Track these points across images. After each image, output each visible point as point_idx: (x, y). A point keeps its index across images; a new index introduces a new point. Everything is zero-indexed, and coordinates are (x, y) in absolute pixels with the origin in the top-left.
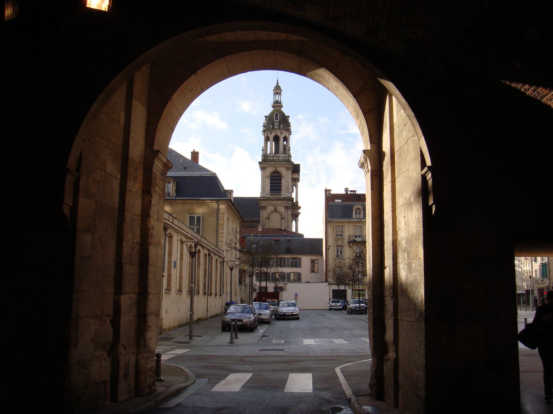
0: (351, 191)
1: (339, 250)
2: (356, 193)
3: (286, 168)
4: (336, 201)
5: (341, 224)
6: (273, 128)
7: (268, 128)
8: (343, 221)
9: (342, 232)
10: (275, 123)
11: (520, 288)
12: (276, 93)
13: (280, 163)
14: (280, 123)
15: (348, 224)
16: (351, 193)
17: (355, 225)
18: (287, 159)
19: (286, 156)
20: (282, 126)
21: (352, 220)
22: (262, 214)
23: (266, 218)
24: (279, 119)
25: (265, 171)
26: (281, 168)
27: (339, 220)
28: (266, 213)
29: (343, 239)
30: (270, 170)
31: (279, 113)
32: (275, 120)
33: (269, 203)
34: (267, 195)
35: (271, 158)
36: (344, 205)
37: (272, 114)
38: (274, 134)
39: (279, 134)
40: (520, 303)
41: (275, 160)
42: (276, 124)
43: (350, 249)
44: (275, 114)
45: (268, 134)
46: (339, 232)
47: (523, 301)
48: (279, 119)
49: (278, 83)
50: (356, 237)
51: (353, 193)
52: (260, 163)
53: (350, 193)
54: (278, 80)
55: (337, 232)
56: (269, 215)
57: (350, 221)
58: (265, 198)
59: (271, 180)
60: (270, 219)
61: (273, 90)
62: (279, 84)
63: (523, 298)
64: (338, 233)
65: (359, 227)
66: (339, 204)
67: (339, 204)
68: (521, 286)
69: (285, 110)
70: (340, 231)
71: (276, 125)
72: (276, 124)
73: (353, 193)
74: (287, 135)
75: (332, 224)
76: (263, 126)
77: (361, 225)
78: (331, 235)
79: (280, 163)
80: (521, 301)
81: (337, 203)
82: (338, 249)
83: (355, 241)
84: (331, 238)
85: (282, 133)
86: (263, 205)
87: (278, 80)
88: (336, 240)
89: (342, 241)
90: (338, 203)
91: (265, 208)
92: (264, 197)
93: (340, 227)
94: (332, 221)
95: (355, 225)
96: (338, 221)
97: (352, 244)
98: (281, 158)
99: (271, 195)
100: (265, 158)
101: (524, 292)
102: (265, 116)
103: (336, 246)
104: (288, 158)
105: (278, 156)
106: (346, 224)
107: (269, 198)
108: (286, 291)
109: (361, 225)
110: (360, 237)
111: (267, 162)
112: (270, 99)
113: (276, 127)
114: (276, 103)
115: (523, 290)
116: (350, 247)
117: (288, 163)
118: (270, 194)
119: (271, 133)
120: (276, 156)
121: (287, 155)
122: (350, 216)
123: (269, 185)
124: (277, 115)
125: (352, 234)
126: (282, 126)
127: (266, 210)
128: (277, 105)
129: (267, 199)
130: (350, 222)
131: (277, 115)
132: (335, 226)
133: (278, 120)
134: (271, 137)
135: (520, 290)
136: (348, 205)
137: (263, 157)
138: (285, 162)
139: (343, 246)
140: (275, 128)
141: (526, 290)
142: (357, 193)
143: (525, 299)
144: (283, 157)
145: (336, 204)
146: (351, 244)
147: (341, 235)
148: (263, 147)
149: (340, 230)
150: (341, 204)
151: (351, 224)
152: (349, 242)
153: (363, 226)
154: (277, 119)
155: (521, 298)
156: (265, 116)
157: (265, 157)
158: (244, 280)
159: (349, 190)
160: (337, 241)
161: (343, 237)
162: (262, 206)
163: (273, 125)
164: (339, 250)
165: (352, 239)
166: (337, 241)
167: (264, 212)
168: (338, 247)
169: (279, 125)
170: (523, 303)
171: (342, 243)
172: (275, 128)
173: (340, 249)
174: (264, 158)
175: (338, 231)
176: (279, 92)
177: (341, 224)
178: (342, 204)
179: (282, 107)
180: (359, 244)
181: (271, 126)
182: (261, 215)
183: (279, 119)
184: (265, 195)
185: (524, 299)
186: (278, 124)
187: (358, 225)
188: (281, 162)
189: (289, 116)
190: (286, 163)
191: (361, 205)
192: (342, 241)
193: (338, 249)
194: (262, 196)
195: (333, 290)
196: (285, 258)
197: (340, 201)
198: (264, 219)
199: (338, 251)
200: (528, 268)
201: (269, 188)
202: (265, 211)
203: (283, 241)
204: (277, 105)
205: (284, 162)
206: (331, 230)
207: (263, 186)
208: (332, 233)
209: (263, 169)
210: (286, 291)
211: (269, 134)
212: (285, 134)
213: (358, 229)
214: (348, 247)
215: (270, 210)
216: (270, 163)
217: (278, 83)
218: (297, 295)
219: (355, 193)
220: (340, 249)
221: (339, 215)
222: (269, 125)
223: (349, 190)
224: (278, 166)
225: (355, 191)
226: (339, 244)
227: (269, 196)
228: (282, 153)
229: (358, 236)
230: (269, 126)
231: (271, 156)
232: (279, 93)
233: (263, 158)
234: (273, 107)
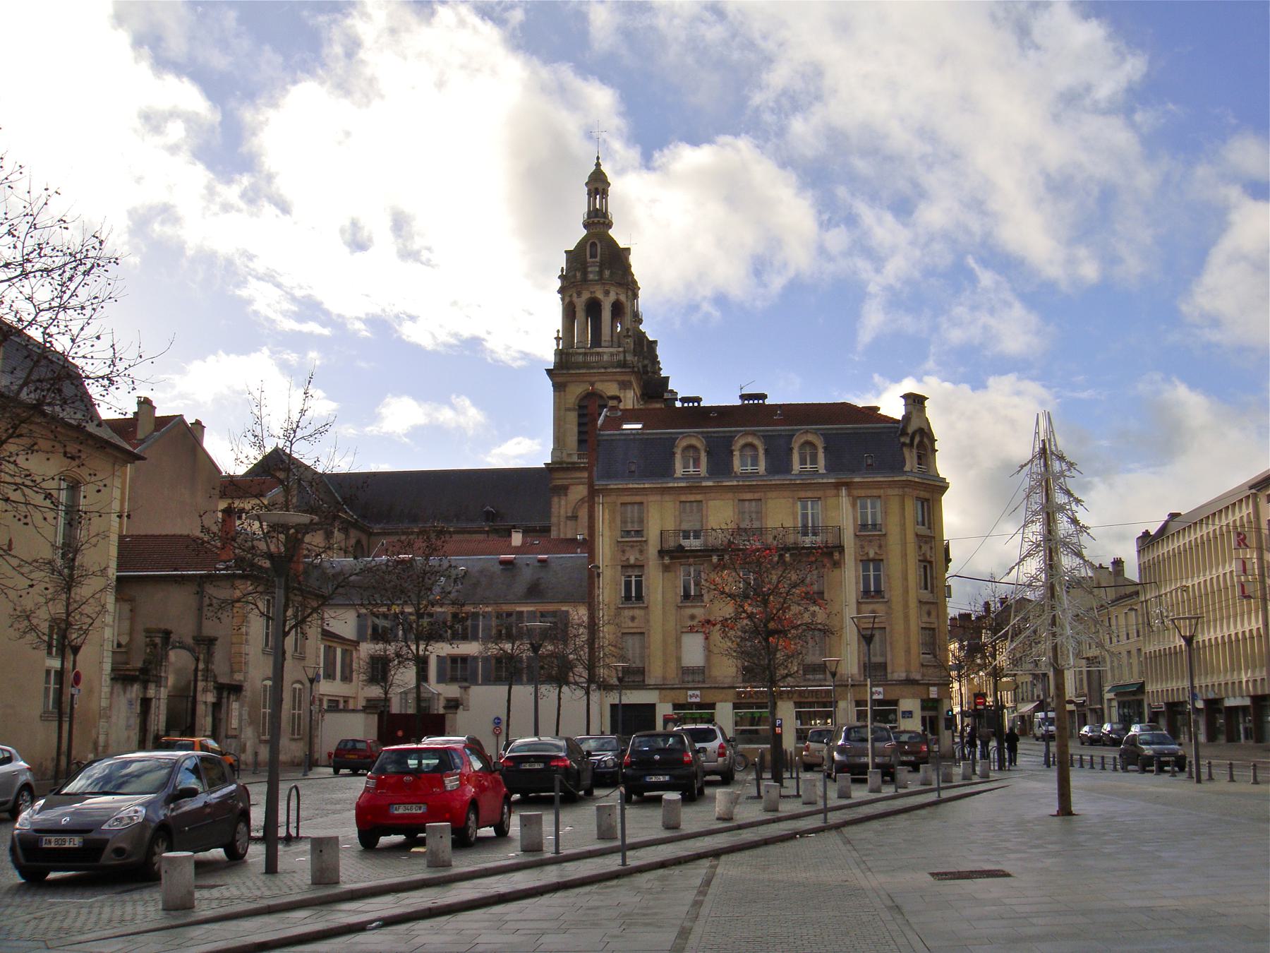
0: (684, 400)
1: (633, 579)
2: (699, 404)
3: (619, 384)
4: (625, 427)
5: (638, 499)
6: (585, 280)
7: (572, 280)
8: (642, 486)
9: (641, 521)
10: (591, 266)
11: (1233, 689)
12: (593, 190)
13: (603, 370)
14: (602, 266)
15: (658, 498)
16: (686, 405)
17: (683, 498)
18: (622, 359)
19: (620, 352)
20: (607, 273)
21: (671, 485)
22: (557, 506)
23: (568, 518)
24: (599, 257)
25: (562, 393)
26: (606, 384)
27: (631, 486)
28: (566, 505)
29: (644, 545)
30: (576, 391)
31: (600, 242)
32: (589, 260)
33: (577, 478)
34: (569, 455)
35: (580, 359)
36: (647, 439)
37: (582, 245)
38: (586, 296)
39: (600, 295)
40: (1240, 738)
41: (591, 362)
42: (593, 272)
43: (666, 574)
44: (589, 244)
45: (571, 296)
46: (633, 522)
47: (1246, 729)
48: (601, 257)
49: (598, 165)
50: (686, 537)
51: (691, 404)
52: (549, 372)
53: (683, 405)
54: (598, 158)
55: (624, 522)
56: (575, 507)
57: (664, 485)
58: (565, 466)
59: (580, 416)
60: (579, 520)
61: (587, 184)
62: (602, 168)
63: (1245, 721)
64: (629, 525)
65: (695, 504)
66: (634, 434)
67: (632, 437)
68: (1223, 685)
69: (620, 236)
70: (636, 519)
71: (591, 272)
72: (593, 272)
73: (691, 404)
74: (623, 298)
75: (608, 499)
76: (559, 277)
77: (699, 497)
78: (607, 533)
79: (603, 370)
80: (1239, 730)
81: (627, 432)
82: (630, 576)
83: (681, 548)
84: (607, 540)
85: (607, 293)
86: (559, 482)
87: (598, 158)
88: (621, 546)
89: (641, 552)
90: (629, 431)
91: (563, 490)
92: (561, 463)
93: (636, 507)
94: (607, 489)
95: (683, 498)
96: (625, 487)
97: (672, 558)
98: (606, 358)
99: (580, 456)
100: (564, 360)
101: (1247, 702)
102: (566, 252)
103: (622, 566)
104: (625, 357)
105: (598, 354)
106: (652, 498)
107: (573, 463)
108: (467, 709)
109: (699, 497)
110: (697, 536)
111: (568, 369)
112: (580, 205)
113: (591, 276)
114: (593, 215)
115: (1242, 697)
116: (666, 569)
117: (623, 370)
118: (578, 455)
119: (579, 294)
120: (592, 354)
121: (621, 349)
122: (668, 472)
123: (575, 429)
124: (594, 245)
125: (670, 525)
126: (607, 273)
127: (566, 495)
128: (598, 221)
129: (568, 468)
130: (664, 491)
131: (594, 245)
132: (619, 505)
133: (598, 259)
134: (580, 303)
135: (1235, 697)
136: (662, 436)
137: (558, 357)
138: (616, 368)
139: (643, 566)
140: (589, 279)
141: (1252, 694)
142: (702, 404)
143: (1251, 725)
144: (612, 354)
145: (623, 437)
146: (667, 560)
147: (638, 531)
148: (558, 331)
149: (636, 515)
150: (637, 437)
151: (667, 498)
152: (662, 553)
153: (707, 503)
154: (593, 256)
155: (1241, 720)
156: (566, 252)
157: (564, 356)
158: (203, 670)
159: (679, 397)
160: (623, 551)
161: (644, 539)
162: (555, 486)
163: (585, 273)
164: (633, 579)
165: (671, 543)
166: (623, 551)
167: (563, 502)
168: (630, 570)
169: (601, 273)
170: (1246, 738)
171: (638, 556)
172: (589, 279)
173: (636, 576)
174: (561, 358)
175: (629, 520)
176: (600, 187)
177: (638, 499)
178: (640, 437)
179: (610, 225)
180: (695, 557)
181: (578, 274)
182: (554, 510)
183: (599, 257)
184: (564, 454)
185: (1247, 725)
186: (597, 269)
187: (691, 498)
188: (605, 368)
189: (628, 250)
190: (618, 370)
191: (699, 436)
192: (641, 552)
193: (630, 576)
194: (555, 459)
195: (613, 707)
196: (522, 612)
197: (639, 426)
198: (562, 519)
199: (628, 584)
200: (1254, 626)
201: (575, 438)
202: (564, 498)
203: (528, 565)
204: (596, 220)
205: (613, 367)
206: (607, 516)
207: (559, 431)
208: (610, 527)
209: (559, 387)
210: (467, 709)
211: (575, 295)
212: (617, 294)
213: (692, 511)
214: (661, 570)
215: (579, 497)
216: (578, 372)
217: (598, 165)
218: (499, 723)
219: (696, 404)
220: (636, 576)
221: (633, 469)
222: (573, 273)
223: (679, 397)
224: (596, 378)
225: (698, 400)
226: (632, 561)
227: (575, 459)
228: (606, 344)
229: (692, 534)
230: (575, 276)
231: (580, 354)
232: (600, 189)
233: (557, 360)
234: (586, 226)
